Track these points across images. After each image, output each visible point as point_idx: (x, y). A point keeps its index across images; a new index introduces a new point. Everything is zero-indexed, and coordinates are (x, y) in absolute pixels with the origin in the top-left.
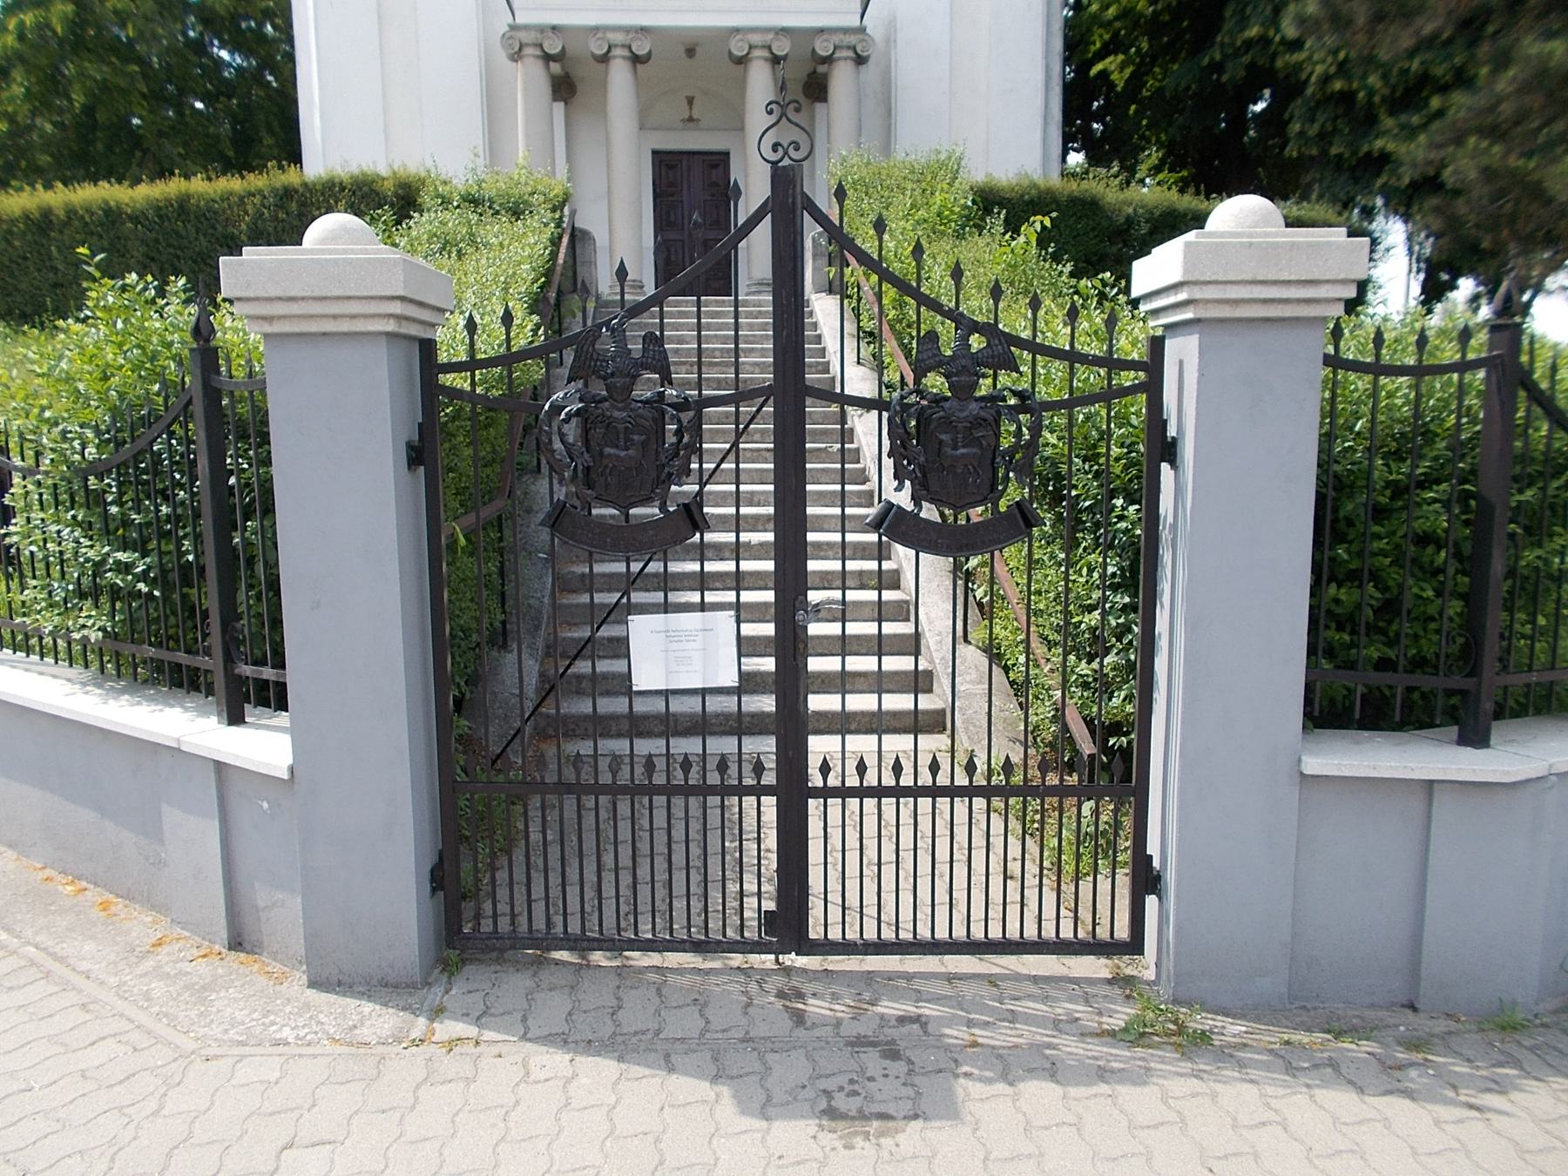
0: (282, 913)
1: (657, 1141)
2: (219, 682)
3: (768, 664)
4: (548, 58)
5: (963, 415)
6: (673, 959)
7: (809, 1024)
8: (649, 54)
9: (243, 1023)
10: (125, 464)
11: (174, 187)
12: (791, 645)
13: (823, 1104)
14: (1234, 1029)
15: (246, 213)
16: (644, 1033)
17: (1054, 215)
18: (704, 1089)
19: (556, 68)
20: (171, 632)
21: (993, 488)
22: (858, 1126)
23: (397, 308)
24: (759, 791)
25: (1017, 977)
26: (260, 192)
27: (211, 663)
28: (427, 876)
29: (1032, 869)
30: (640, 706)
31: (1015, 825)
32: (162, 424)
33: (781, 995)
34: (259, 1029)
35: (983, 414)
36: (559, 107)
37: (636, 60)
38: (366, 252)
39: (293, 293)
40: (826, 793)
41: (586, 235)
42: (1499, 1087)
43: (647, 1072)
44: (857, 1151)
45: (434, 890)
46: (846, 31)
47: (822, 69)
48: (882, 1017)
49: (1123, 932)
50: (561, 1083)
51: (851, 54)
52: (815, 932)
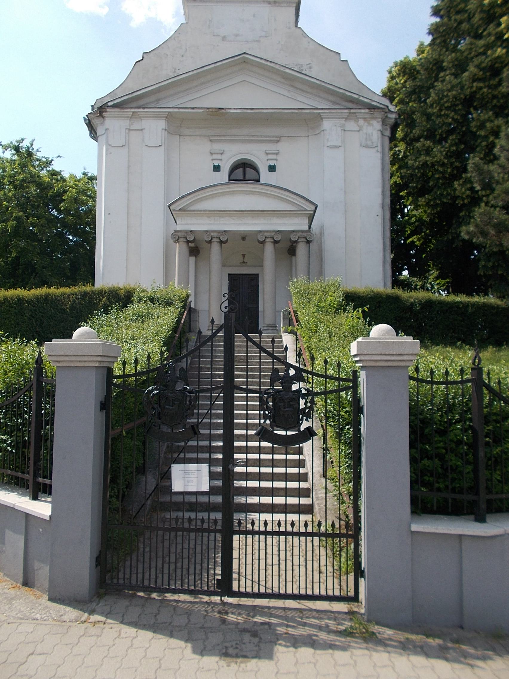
0: (42, 572)
1: (160, 660)
2: (31, 484)
3: (219, 483)
4: (188, 242)
5: (286, 397)
6: (183, 597)
7: (227, 623)
8: (227, 240)
9: (23, 612)
10: (8, 405)
11: (44, 290)
12: (228, 476)
13: (224, 651)
14: (389, 632)
15: (70, 301)
16: (165, 623)
17: (368, 306)
18: (182, 644)
20: (17, 465)
21: (298, 422)
22: (234, 659)
23: (99, 359)
24: (216, 531)
25: (311, 610)
26: (76, 293)
27: (28, 477)
28: (95, 560)
29: (330, 569)
30: (175, 499)
31: (330, 553)
32: (23, 392)
33: (219, 612)
34: (28, 614)
35: (294, 397)
37: (221, 242)
38: (91, 341)
39: (67, 354)
40: (240, 533)
42: (484, 658)
43: (163, 637)
44: (231, 667)
45: (97, 566)
46: (302, 231)
47: (294, 244)
48: (255, 622)
49: (352, 593)
50: (131, 639)
51: (305, 240)
52: (235, 587)
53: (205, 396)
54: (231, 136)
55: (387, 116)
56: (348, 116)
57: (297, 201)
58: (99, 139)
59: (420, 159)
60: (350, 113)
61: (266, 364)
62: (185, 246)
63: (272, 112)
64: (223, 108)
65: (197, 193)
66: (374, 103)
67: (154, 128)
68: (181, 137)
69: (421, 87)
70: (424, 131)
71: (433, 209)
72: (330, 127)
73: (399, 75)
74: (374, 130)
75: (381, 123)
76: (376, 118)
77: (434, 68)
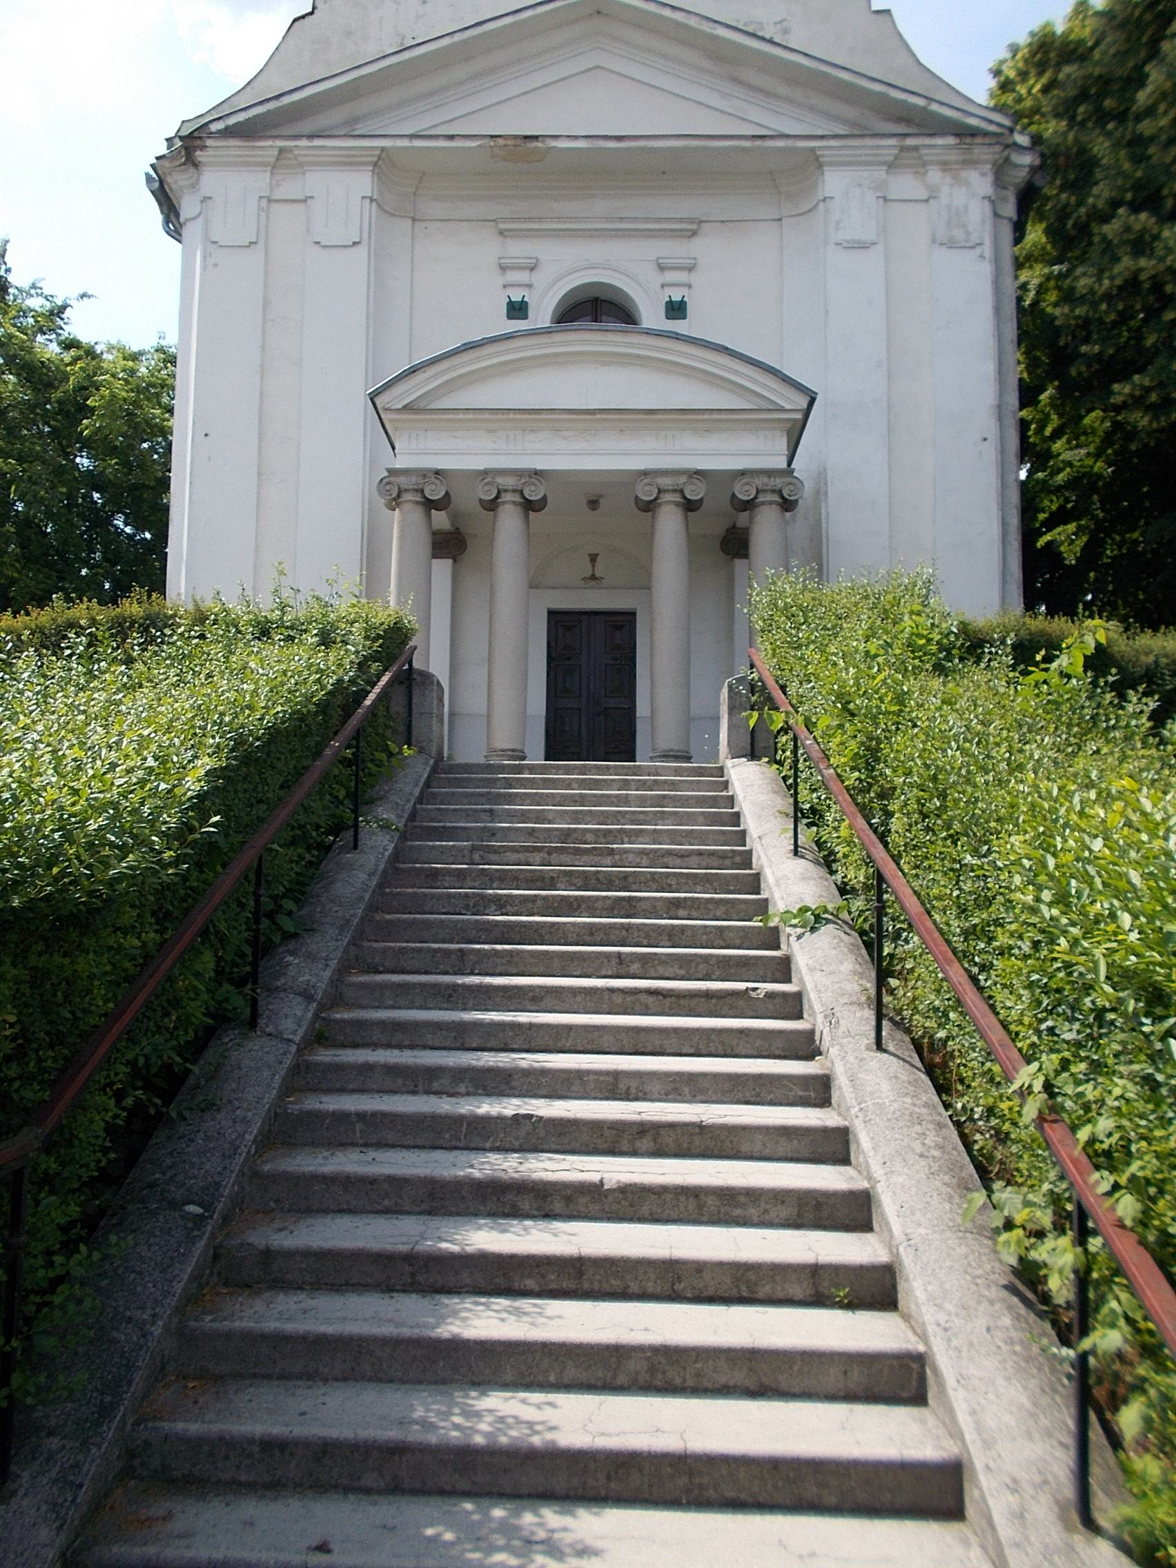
4: (430, 505)
8: (544, 498)
19: (441, 519)
36: (442, 569)
37: (529, 506)
41: (427, 677)
51: (777, 498)
53: (435, 985)
54: (559, 219)
55: (1007, 159)
56: (896, 157)
57: (755, 381)
58: (185, 232)
59: (1118, 269)
60: (903, 149)
61: (678, 861)
62: (417, 515)
63: (675, 148)
64: (536, 138)
65: (456, 360)
66: (973, 121)
67: (340, 194)
68: (417, 224)
69: (1105, 82)
70: (1126, 191)
71: (1156, 417)
72: (846, 190)
73: (1023, 75)
74: (970, 199)
75: (990, 178)
76: (977, 162)
77: (1148, 17)
